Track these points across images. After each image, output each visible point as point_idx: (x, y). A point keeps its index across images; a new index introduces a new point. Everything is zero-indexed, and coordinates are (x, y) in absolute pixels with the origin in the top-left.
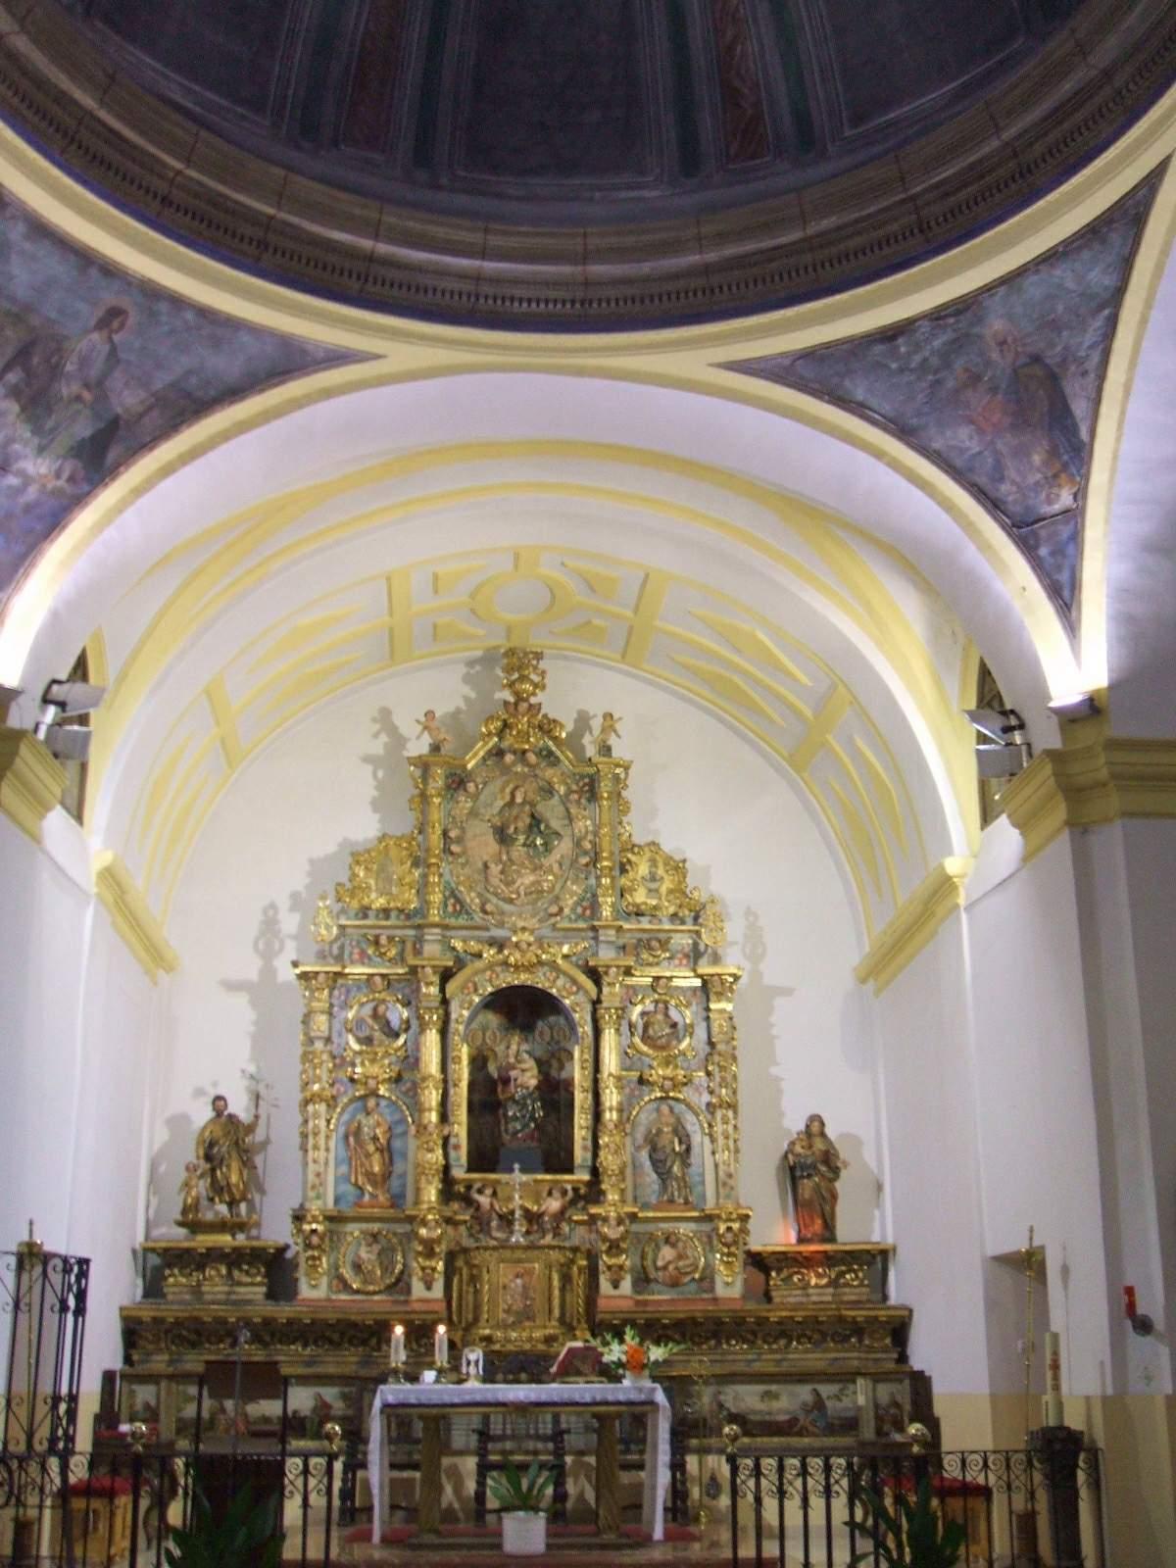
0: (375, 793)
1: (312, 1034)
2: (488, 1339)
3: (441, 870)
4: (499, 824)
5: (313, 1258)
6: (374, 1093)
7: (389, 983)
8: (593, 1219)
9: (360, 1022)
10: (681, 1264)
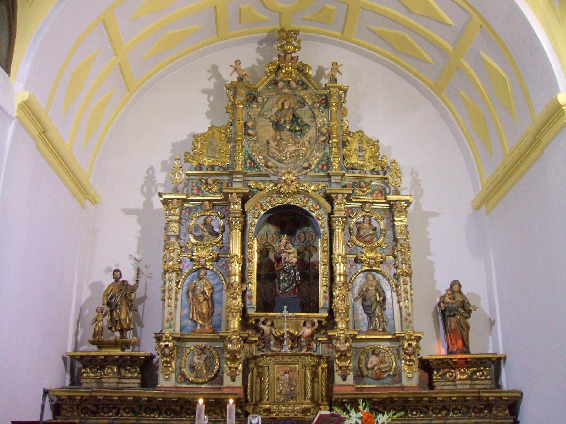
0: (209, 109)
1: (169, 234)
2: (268, 411)
3: (243, 144)
4: (276, 120)
5: (167, 362)
6: (204, 267)
7: (213, 206)
8: (330, 338)
9: (196, 228)
10: (382, 366)
